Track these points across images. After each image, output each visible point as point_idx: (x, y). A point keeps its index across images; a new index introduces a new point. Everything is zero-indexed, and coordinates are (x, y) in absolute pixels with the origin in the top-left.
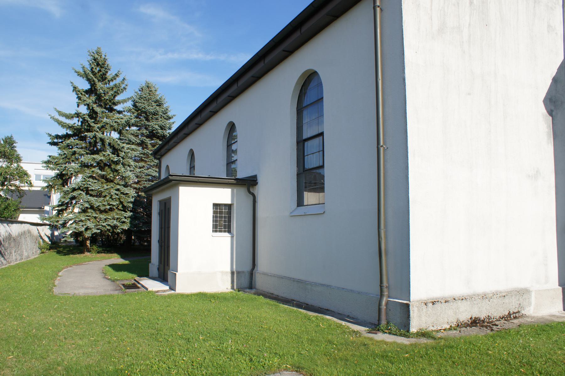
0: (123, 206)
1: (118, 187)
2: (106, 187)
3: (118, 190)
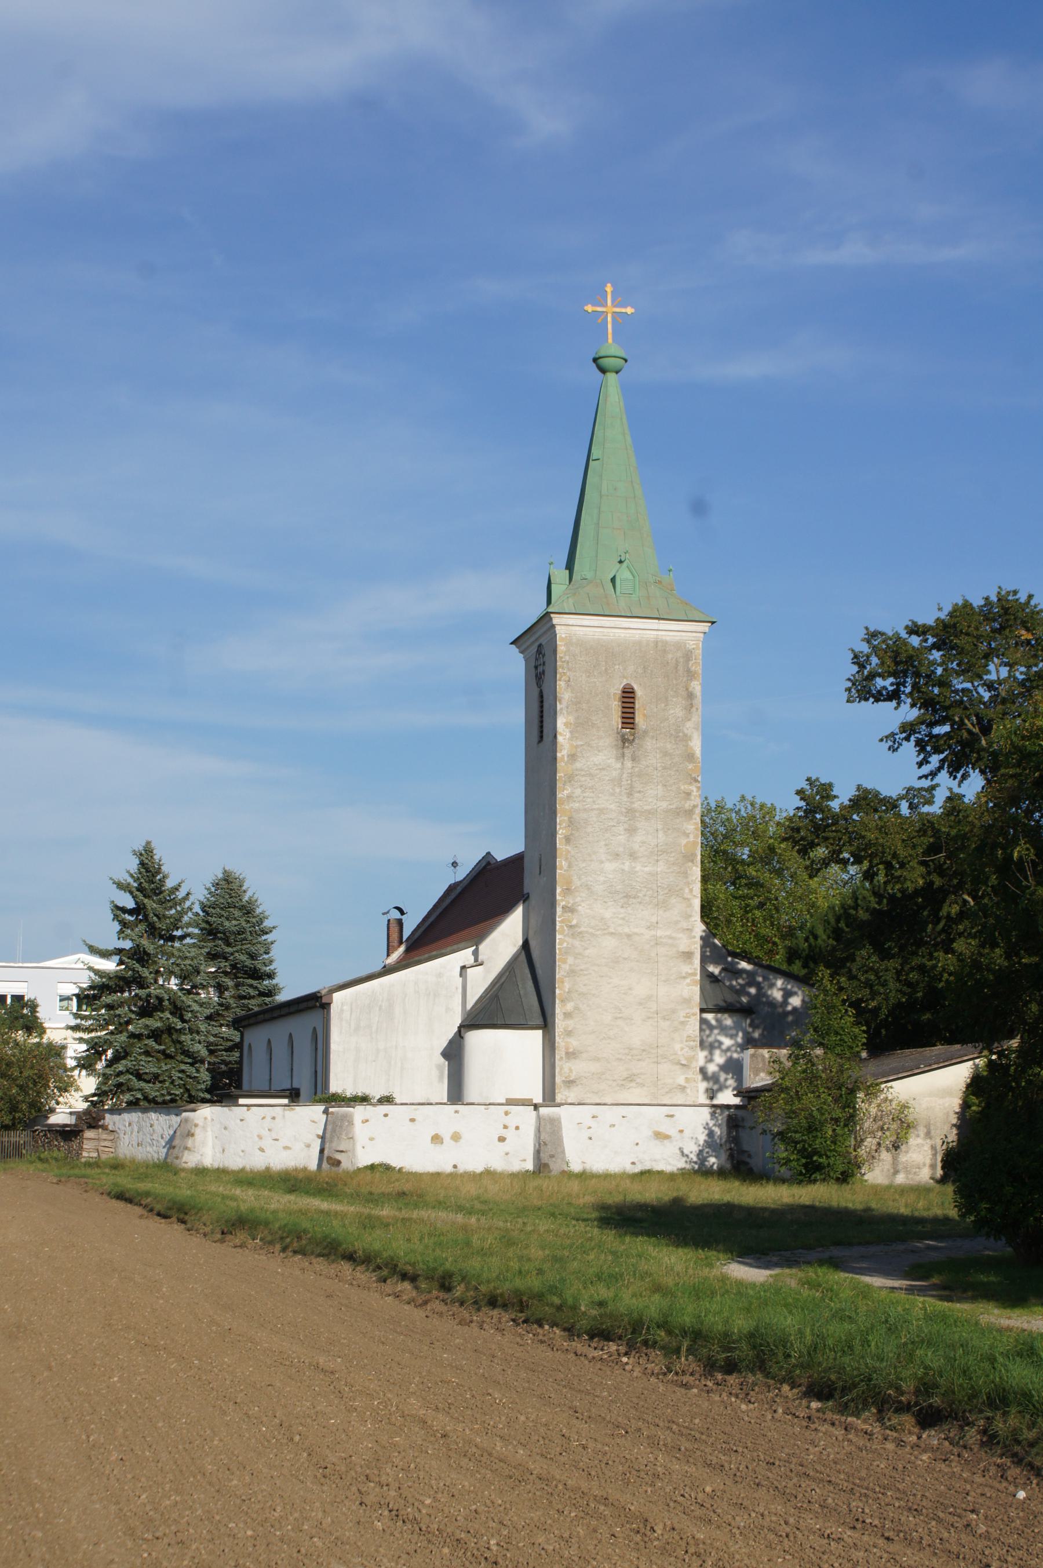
0: (190, 1096)
1: (183, 1067)
2: (165, 1068)
3: (183, 1071)
